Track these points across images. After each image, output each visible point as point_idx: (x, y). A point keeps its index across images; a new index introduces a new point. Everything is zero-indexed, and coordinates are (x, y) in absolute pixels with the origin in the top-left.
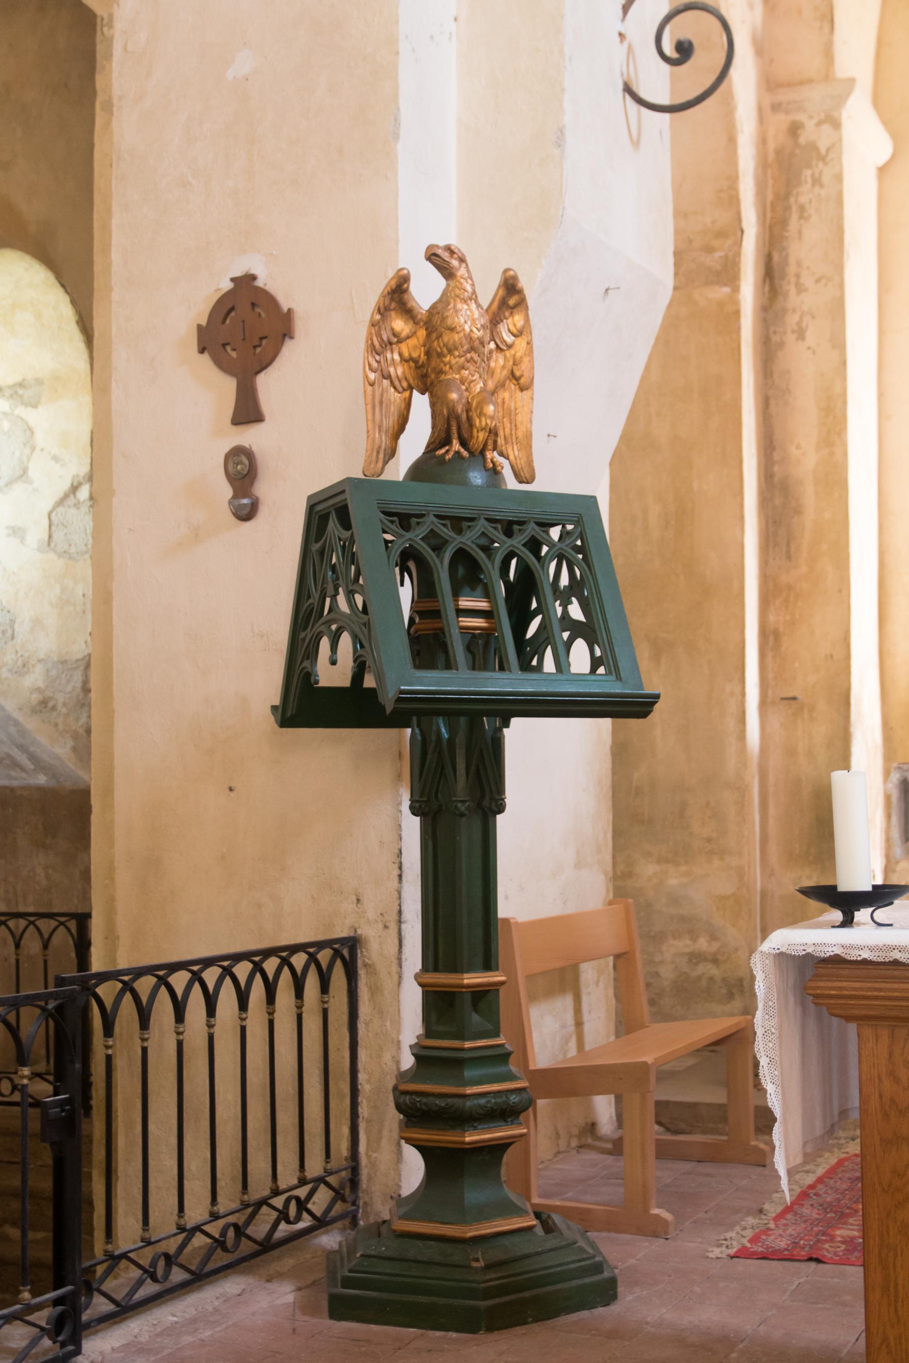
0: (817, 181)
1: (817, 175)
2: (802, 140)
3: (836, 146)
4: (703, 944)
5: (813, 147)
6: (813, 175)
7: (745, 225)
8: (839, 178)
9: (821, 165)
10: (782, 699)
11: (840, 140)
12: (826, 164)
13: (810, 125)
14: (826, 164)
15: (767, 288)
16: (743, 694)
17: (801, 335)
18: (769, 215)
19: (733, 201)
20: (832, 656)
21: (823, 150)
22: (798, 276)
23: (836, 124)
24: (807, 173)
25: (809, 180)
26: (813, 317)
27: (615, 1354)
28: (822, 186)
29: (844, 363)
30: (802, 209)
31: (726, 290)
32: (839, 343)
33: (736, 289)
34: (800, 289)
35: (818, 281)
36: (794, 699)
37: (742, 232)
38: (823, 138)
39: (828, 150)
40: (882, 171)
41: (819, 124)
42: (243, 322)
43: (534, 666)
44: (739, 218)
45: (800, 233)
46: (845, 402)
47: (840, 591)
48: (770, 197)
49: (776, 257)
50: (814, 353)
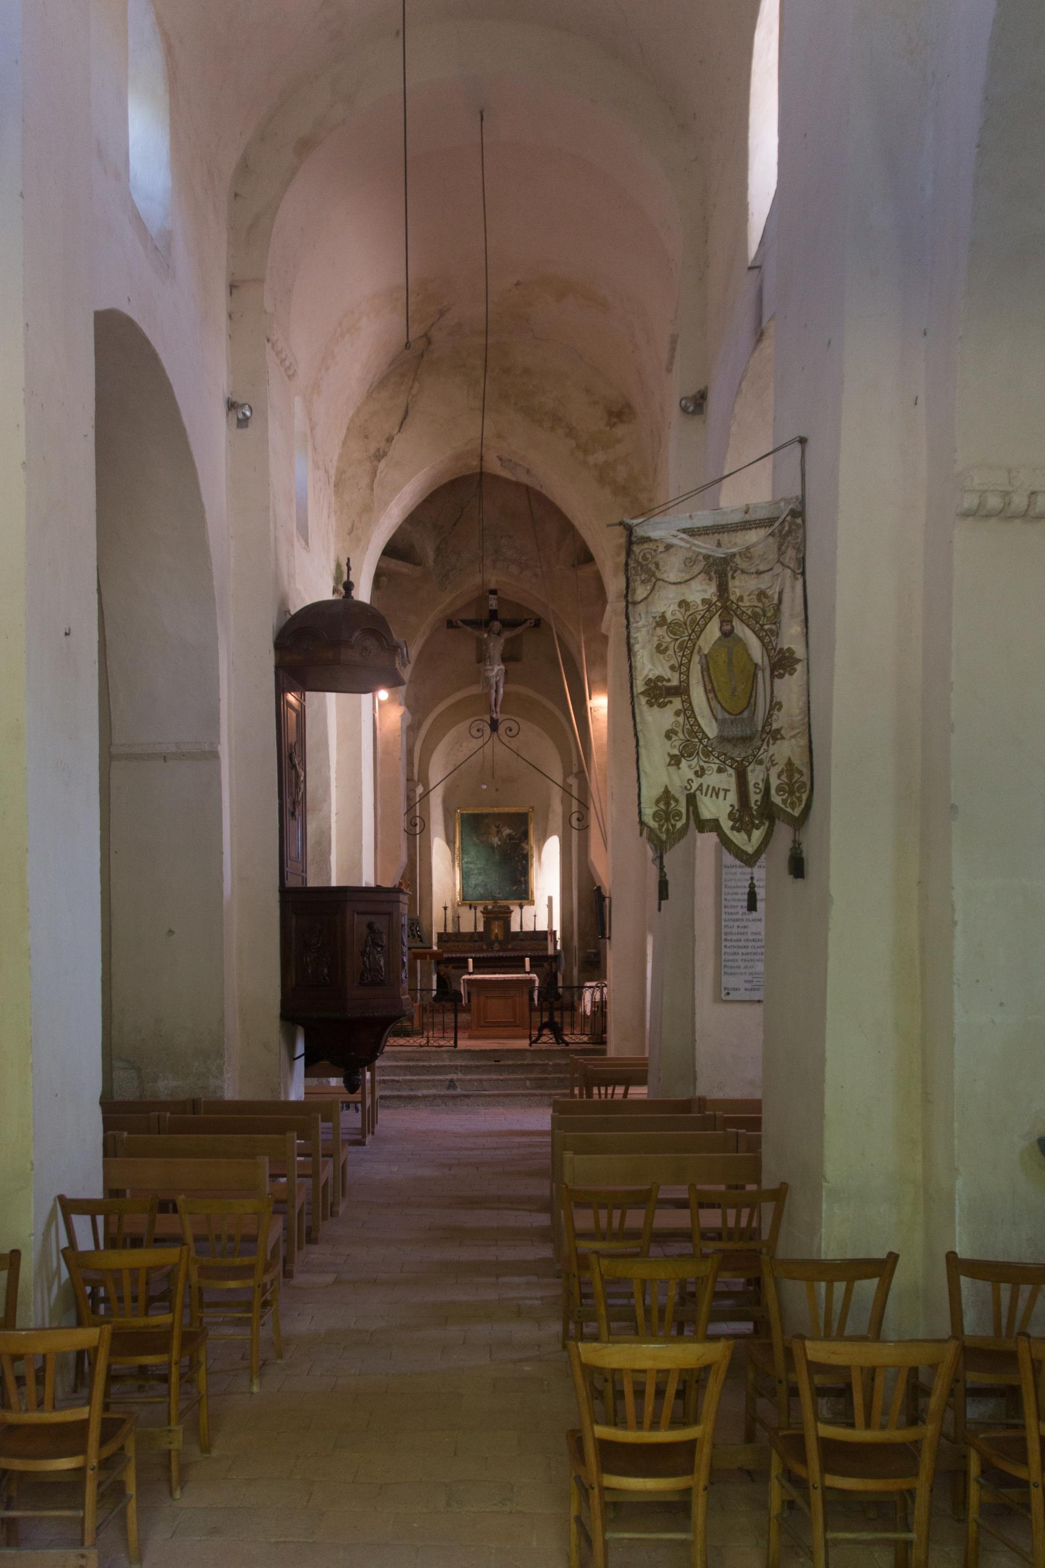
42: (535, 916)
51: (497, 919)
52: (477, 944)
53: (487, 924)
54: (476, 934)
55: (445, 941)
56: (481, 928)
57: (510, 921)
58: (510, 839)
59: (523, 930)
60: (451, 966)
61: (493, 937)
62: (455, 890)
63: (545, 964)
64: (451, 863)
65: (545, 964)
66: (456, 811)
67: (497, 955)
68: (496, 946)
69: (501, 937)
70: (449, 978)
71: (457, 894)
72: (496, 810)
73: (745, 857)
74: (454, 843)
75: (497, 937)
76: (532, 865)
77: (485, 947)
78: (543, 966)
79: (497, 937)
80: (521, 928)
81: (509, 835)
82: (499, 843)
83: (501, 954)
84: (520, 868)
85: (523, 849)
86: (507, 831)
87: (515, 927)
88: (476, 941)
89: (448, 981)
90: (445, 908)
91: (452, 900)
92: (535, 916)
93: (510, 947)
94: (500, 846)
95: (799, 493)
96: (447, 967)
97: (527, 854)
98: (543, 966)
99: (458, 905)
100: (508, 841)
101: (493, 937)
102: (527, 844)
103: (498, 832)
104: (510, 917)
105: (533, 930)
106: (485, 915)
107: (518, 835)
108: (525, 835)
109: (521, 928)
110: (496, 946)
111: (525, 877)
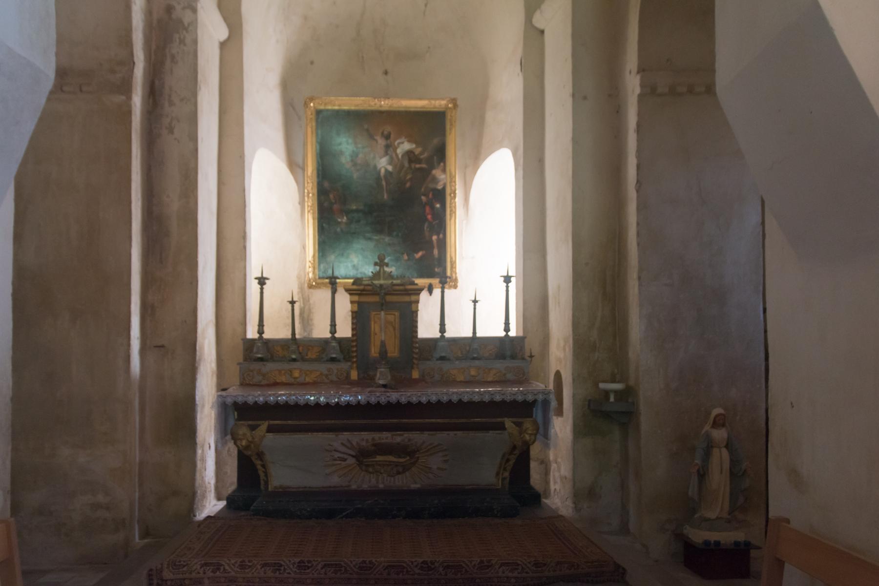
0: (182, 42)
1: (182, 37)
2: (174, 16)
3: (194, 23)
4: (101, 498)
5: (180, 21)
6: (180, 38)
7: (136, 60)
8: (195, 42)
9: (184, 32)
10: (155, 347)
11: (196, 20)
12: (187, 32)
13: (178, 8)
14: (187, 32)
15: (151, 100)
16: (129, 345)
17: (171, 131)
18: (153, 57)
19: (127, 42)
20: (185, 321)
21: (186, 24)
22: (170, 96)
23: (194, 11)
24: (176, 36)
25: (178, 40)
26: (178, 121)
27: (552, 566)
28: (185, 45)
29: (196, 150)
30: (173, 57)
31: (123, 98)
32: (194, 138)
33: (129, 98)
34: (171, 103)
35: (182, 100)
36: (163, 346)
37: (134, 63)
38: (187, 17)
39: (189, 25)
40: (223, 45)
41: (184, 8)
42: (475, 302)
43: (612, 402)
44: (132, 54)
45: (172, 70)
46: (196, 173)
47: (191, 283)
48: (154, 47)
49: (157, 82)
50: (178, 142)
51: (383, 305)
52: (334, 366)
53: (359, 318)
54: (334, 344)
55: (261, 360)
56: (345, 330)
57: (416, 312)
58: (410, 161)
59: (447, 335)
60: (264, 426)
61: (374, 352)
62: (305, 258)
63: (508, 423)
64: (298, 207)
65: (508, 423)
66: (306, 105)
67: (383, 400)
68: (382, 376)
69: (393, 351)
70: (260, 455)
71: (308, 264)
72: (385, 104)
73: (507, 322)
74: (303, 169)
75: (383, 353)
76: (453, 212)
77: (354, 375)
78: (501, 427)
79: (383, 353)
80: (442, 329)
81: (409, 153)
82: (390, 168)
83: (394, 396)
84: (429, 217)
85: (435, 180)
86: (405, 146)
87: (427, 329)
88: (333, 360)
89: (258, 463)
90: (292, 303)
91: (299, 277)
92: (475, 302)
93: (324, 225)
94: (391, 173)
95: (446, 291)
96: (253, 428)
97: (444, 190)
98: (501, 427)
99: (311, 287)
100: (406, 164)
101: (374, 352)
102: (444, 171)
103: (387, 147)
104: (417, 302)
105: (470, 334)
106: (356, 298)
107: (425, 155)
108: (440, 154)
109: (442, 329)
110: (382, 376)
111: (438, 234)
